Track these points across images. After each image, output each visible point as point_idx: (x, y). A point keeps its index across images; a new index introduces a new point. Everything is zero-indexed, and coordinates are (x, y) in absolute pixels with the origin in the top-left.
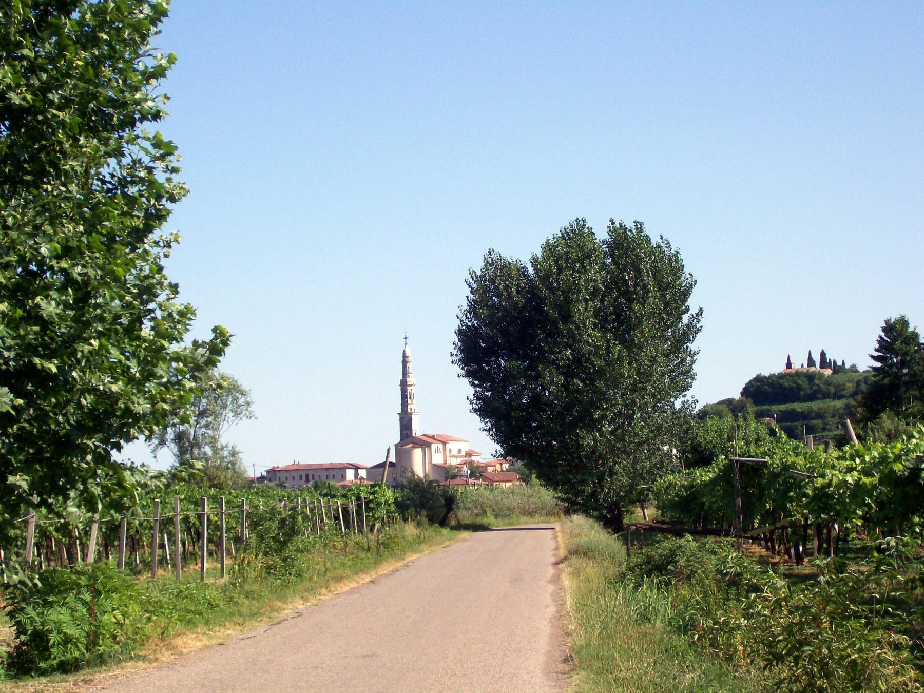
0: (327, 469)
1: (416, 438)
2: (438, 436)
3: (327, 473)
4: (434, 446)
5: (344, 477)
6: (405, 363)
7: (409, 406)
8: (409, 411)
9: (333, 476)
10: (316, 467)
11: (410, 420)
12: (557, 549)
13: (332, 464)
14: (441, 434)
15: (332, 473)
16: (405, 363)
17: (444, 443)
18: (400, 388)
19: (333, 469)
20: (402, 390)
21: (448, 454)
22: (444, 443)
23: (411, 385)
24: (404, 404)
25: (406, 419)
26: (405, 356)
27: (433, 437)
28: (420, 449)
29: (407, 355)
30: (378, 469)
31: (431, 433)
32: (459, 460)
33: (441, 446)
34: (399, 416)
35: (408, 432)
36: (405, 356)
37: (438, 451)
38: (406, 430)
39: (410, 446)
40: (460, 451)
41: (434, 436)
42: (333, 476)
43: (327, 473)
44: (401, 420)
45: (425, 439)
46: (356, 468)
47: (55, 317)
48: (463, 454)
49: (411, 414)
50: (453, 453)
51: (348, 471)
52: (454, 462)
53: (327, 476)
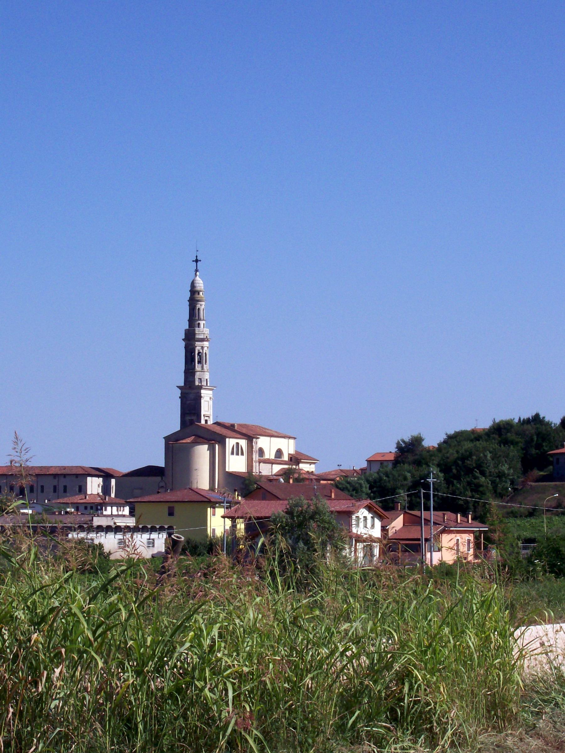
0: (55, 476)
1: (205, 429)
2: (240, 425)
3: (55, 482)
4: (230, 443)
5: (82, 489)
6: (193, 301)
7: (198, 375)
8: (197, 383)
9: (65, 487)
10: (74, 472)
11: (198, 398)
12: (456, 600)
13: (65, 468)
14: (247, 423)
15: (63, 482)
16: (193, 301)
17: (250, 439)
18: (183, 344)
19: (65, 476)
20: (186, 347)
21: (256, 457)
22: (250, 439)
23: (202, 340)
24: (190, 372)
25: (192, 396)
26: (194, 291)
27: (231, 428)
28: (206, 447)
29: (198, 289)
30: (129, 478)
31: (227, 420)
32: (277, 468)
33: (243, 443)
34: (179, 391)
35: (194, 418)
36: (194, 291)
37: (237, 450)
38: (190, 414)
39: (188, 440)
40: (279, 453)
41: (233, 426)
42: (65, 487)
43: (55, 482)
44: (183, 397)
45: (218, 429)
46: (106, 475)
47: (401, 443)
48: (286, 458)
49: (200, 388)
50: (267, 456)
51: (89, 479)
52: (266, 470)
53: (55, 487)
